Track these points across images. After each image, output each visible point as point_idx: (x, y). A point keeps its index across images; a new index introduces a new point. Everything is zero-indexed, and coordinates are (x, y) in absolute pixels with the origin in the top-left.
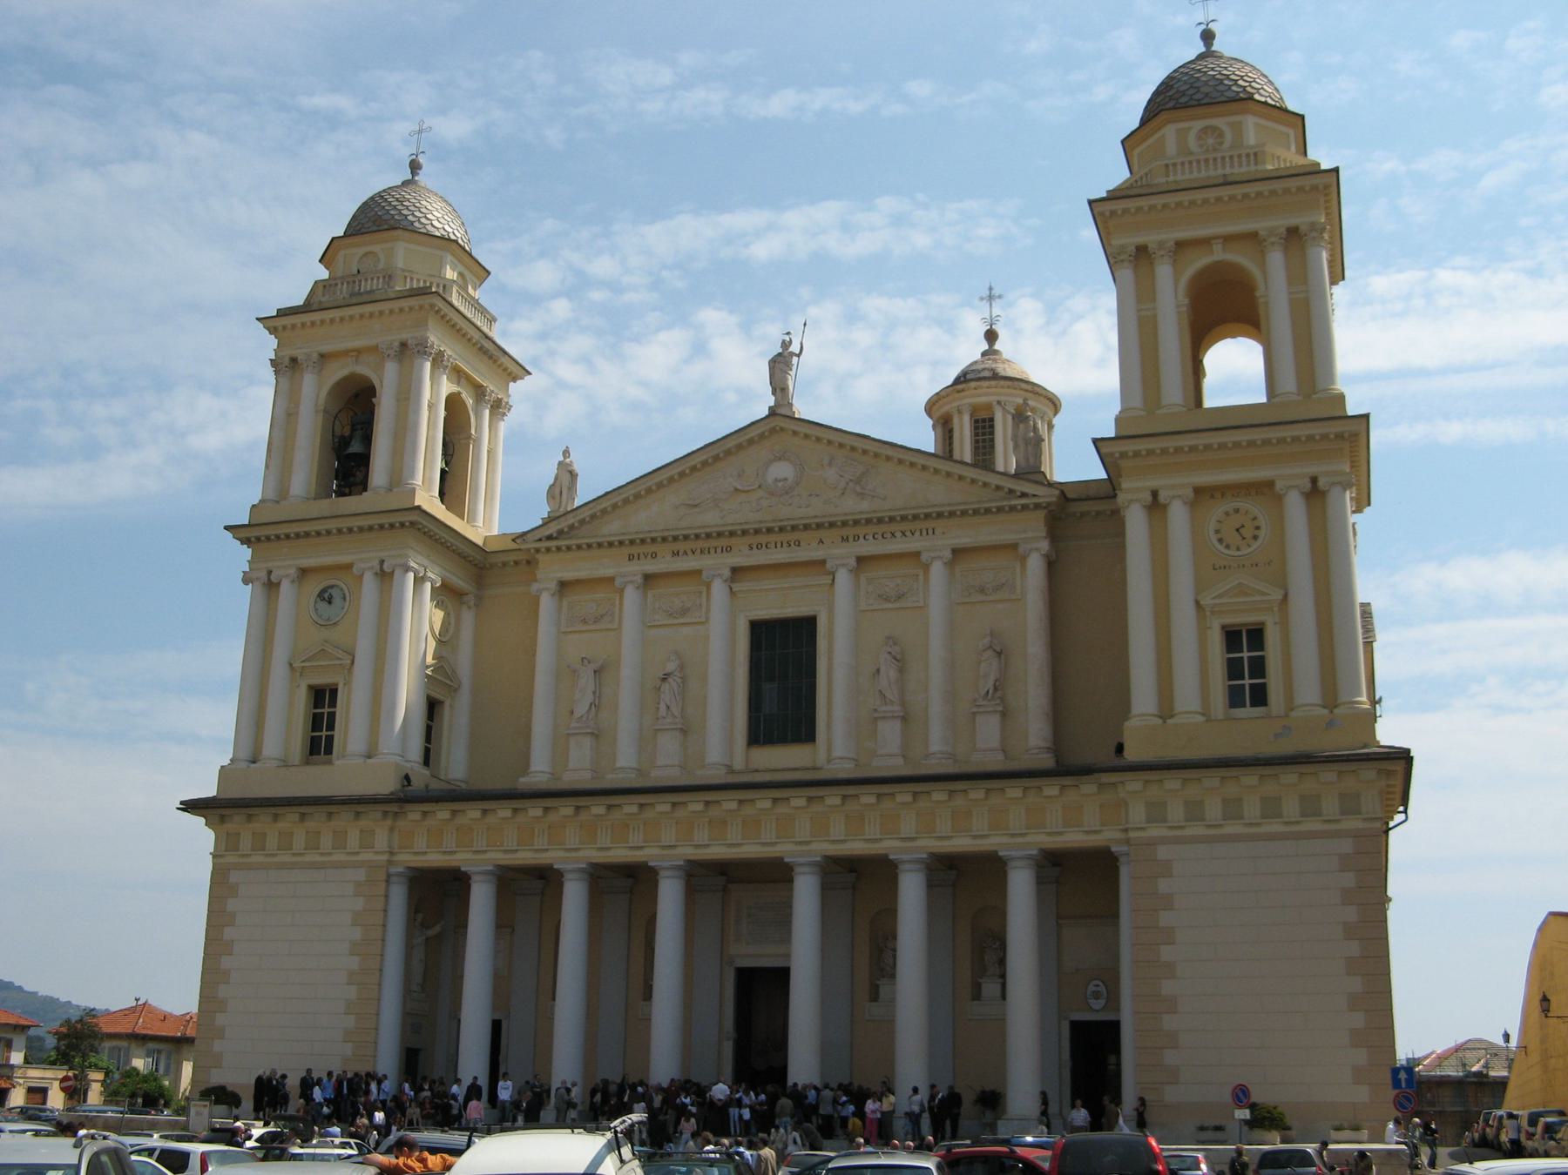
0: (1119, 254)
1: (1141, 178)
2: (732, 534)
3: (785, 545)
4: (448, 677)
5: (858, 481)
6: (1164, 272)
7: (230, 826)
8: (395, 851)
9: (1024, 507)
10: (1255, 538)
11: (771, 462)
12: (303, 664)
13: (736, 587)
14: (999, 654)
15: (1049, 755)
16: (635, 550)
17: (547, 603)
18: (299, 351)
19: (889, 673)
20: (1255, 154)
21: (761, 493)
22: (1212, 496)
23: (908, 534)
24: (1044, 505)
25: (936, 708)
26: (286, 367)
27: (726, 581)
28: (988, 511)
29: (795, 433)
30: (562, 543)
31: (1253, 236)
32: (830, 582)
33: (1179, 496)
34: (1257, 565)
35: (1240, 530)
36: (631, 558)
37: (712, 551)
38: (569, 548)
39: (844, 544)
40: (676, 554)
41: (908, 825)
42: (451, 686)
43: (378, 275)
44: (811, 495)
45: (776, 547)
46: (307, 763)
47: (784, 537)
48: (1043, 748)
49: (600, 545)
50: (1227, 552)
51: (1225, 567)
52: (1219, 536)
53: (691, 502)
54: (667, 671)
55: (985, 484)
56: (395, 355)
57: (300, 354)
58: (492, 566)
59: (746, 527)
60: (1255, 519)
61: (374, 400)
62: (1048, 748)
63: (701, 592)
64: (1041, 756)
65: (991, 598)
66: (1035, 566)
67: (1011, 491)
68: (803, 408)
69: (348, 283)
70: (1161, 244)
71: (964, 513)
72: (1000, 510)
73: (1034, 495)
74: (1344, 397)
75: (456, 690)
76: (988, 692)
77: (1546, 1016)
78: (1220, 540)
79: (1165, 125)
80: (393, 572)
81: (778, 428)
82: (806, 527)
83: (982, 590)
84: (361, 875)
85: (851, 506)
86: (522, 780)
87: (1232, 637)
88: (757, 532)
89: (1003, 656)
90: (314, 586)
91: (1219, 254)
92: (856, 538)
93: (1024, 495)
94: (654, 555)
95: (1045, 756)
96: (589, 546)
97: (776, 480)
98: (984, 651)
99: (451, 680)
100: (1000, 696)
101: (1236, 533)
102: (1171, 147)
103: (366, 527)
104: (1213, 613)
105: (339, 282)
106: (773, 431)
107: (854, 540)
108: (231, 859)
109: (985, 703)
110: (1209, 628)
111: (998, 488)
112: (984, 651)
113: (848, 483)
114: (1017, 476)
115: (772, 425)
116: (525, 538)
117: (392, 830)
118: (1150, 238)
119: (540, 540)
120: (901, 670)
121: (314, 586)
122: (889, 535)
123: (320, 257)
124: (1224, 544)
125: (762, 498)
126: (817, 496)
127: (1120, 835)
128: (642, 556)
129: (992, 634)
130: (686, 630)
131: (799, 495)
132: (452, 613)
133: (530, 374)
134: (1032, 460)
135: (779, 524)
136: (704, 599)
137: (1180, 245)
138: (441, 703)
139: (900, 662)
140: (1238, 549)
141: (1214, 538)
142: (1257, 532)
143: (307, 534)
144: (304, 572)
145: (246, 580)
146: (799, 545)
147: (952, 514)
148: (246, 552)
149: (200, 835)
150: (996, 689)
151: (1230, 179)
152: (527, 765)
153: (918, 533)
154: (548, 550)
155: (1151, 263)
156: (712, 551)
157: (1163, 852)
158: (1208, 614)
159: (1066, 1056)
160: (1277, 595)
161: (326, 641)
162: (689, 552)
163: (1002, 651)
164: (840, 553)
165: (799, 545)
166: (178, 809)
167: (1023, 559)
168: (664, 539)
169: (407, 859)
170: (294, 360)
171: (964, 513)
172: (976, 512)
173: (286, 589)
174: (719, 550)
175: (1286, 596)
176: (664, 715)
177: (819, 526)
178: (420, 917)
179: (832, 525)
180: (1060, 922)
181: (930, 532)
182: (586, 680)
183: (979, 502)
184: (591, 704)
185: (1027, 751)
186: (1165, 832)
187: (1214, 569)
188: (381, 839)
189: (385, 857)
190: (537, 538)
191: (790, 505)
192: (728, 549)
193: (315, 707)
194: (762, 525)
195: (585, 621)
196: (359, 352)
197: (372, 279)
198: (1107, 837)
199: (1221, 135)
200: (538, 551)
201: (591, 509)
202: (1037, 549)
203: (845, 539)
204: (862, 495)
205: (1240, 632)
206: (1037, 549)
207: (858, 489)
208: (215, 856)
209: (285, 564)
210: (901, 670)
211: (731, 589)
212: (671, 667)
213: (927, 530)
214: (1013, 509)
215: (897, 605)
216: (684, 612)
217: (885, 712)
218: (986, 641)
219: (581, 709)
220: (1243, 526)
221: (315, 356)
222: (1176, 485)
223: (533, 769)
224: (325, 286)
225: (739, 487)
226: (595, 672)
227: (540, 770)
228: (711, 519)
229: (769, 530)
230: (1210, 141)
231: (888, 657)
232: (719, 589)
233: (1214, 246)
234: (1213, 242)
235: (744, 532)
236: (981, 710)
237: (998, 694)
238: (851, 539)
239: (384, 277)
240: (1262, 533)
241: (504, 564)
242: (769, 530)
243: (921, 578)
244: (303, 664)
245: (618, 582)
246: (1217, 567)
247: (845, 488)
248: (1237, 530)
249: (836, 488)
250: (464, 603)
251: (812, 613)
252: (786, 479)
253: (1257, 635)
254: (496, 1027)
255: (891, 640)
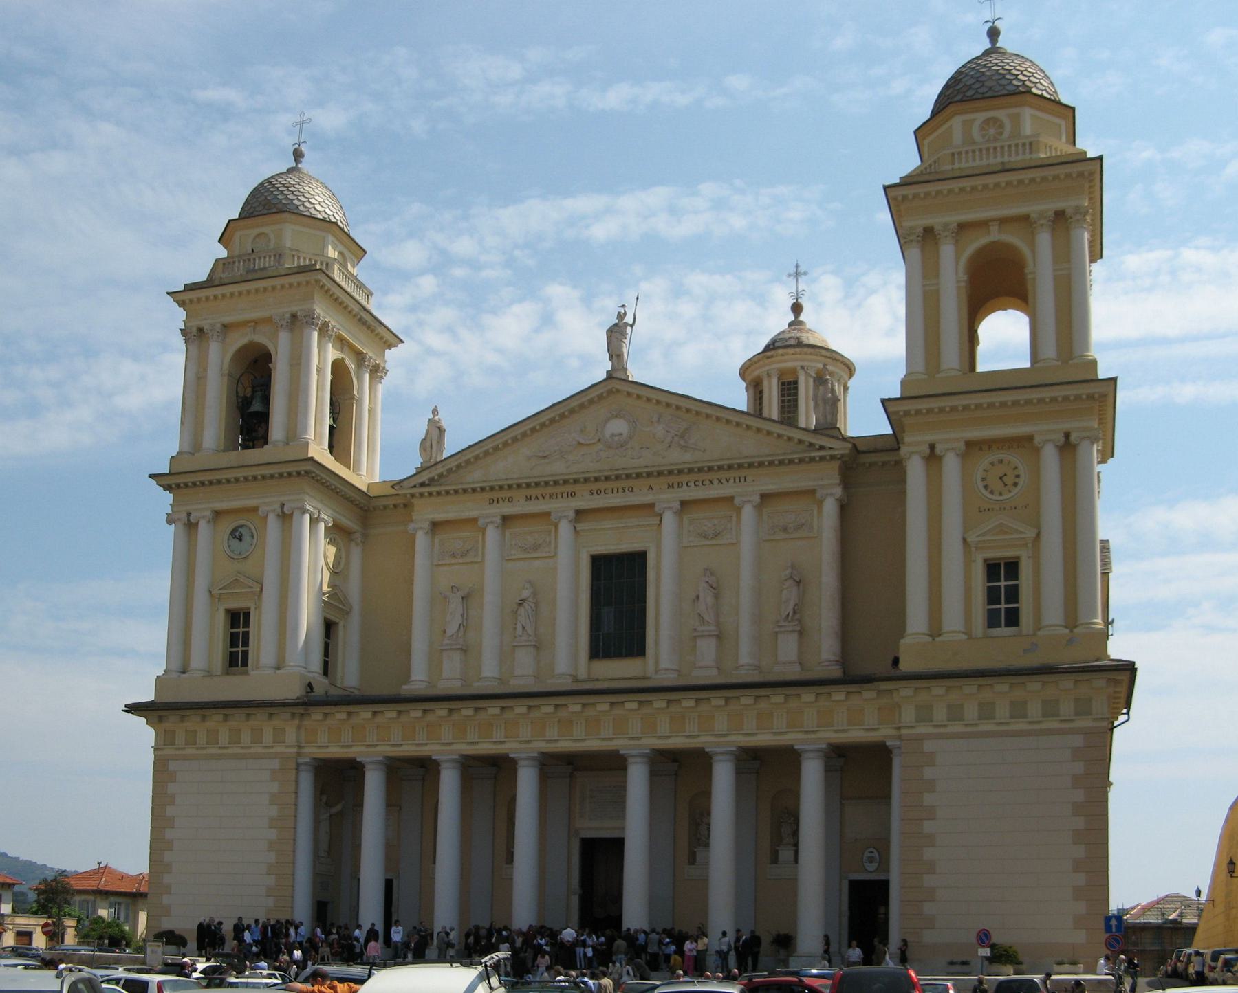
0: (909, 235)
1: (930, 165)
2: (576, 481)
3: (620, 490)
4: (341, 602)
5: (682, 436)
6: (947, 251)
7: (167, 725)
8: (302, 745)
9: (822, 458)
10: (1015, 484)
11: (607, 420)
12: (221, 592)
13: (580, 527)
14: (798, 583)
15: (838, 667)
16: (495, 495)
17: (421, 540)
18: (204, 322)
19: (707, 598)
20: (1031, 144)
21: (600, 446)
22: (981, 449)
23: (724, 481)
24: (839, 456)
25: (745, 628)
26: (195, 336)
27: (571, 521)
28: (791, 462)
29: (629, 394)
30: (433, 489)
31: (1025, 219)
32: (658, 522)
33: (952, 449)
34: (1015, 508)
35: (1003, 478)
36: (491, 502)
37: (559, 496)
38: (439, 493)
39: (671, 490)
40: (529, 498)
41: (721, 724)
42: (343, 610)
43: (269, 254)
44: (642, 448)
45: (613, 493)
46: (228, 674)
47: (620, 484)
48: (833, 661)
49: (465, 491)
50: (990, 496)
51: (989, 510)
52: (985, 483)
53: (540, 454)
54: (523, 597)
55: (789, 439)
56: (287, 326)
57: (205, 324)
58: (375, 508)
59: (587, 475)
60: (1016, 468)
61: (270, 365)
62: (837, 661)
63: (550, 531)
64: (830, 668)
65: (792, 536)
66: (830, 508)
67: (811, 445)
68: (636, 373)
69: (244, 261)
70: (946, 226)
71: (771, 463)
72: (801, 461)
73: (830, 448)
74: (1096, 362)
75: (348, 613)
76: (788, 614)
77: (1232, 876)
78: (986, 487)
79: (953, 116)
80: (292, 513)
81: (614, 390)
82: (638, 476)
83: (785, 529)
84: (275, 764)
85: (677, 457)
86: (404, 687)
87: (992, 569)
88: (597, 479)
89: (801, 585)
90: (227, 526)
91: (995, 235)
92: (680, 485)
93: (822, 448)
94: (511, 500)
95: (833, 667)
96: (456, 492)
97: (613, 435)
98: (786, 580)
99: (344, 605)
100: (798, 619)
101: (999, 480)
102: (957, 137)
103: (268, 475)
104: (977, 549)
105: (236, 260)
106: (610, 392)
107: (678, 487)
108: (169, 751)
109: (786, 624)
110: (974, 561)
111: (800, 442)
112: (786, 580)
113: (673, 438)
114: (817, 431)
115: (609, 387)
116: (402, 484)
117: (299, 727)
118: (935, 221)
119: (415, 486)
120: (717, 597)
121: (227, 526)
122: (708, 482)
123: (218, 238)
124: (989, 490)
125: (601, 450)
126: (648, 448)
127: (893, 732)
128: (500, 500)
129: (793, 567)
130: (537, 563)
131: (632, 448)
132: (343, 549)
133: (403, 342)
134: (829, 417)
135: (616, 473)
136: (553, 537)
137: (962, 226)
138: (336, 624)
139: (716, 590)
140: (1001, 494)
141: (980, 485)
142: (1017, 480)
143: (219, 482)
144: (217, 514)
145: (170, 521)
146: (632, 491)
147: (761, 464)
148: (168, 497)
149: (143, 732)
150: (795, 612)
151: (1008, 167)
152: (409, 676)
153: (732, 481)
154: (422, 495)
155: (937, 243)
156: (559, 496)
157: (928, 746)
158: (973, 549)
159: (845, 907)
160: (1031, 533)
161: (238, 572)
162: (540, 497)
163: (800, 581)
164: (667, 498)
165: (632, 491)
166: (123, 711)
167: (820, 503)
168: (519, 486)
169: (312, 751)
170: (201, 330)
171: (771, 463)
172: (781, 463)
173: (204, 529)
174: (565, 495)
175: (1038, 535)
176: (520, 634)
177: (649, 475)
178: (324, 798)
179: (660, 473)
180: (843, 802)
181: (742, 480)
182: (456, 605)
183: (785, 454)
184: (460, 625)
185: (819, 663)
186: (931, 730)
187: (980, 511)
188: (291, 735)
189: (295, 750)
190: (412, 485)
191: (625, 456)
192: (573, 494)
193: (232, 628)
194: (601, 474)
195: (453, 556)
196: (256, 322)
197: (265, 257)
198: (882, 733)
199: (1001, 126)
200: (413, 496)
201: (456, 460)
202: (832, 495)
203: (671, 486)
204: (685, 448)
205: (999, 565)
206: (832, 495)
207: (682, 443)
208: (156, 749)
209: (202, 508)
210: (717, 597)
211: (575, 528)
212: (525, 594)
213: (740, 478)
214: (812, 460)
215: (714, 542)
216: (536, 547)
217: (702, 631)
218: (788, 572)
219: (452, 629)
220: (1005, 475)
221: (219, 326)
222: (950, 439)
223: (413, 678)
224: (224, 264)
225: (582, 441)
226: (463, 598)
227: (419, 679)
228: (558, 468)
229: (607, 478)
230: (992, 131)
231: (706, 585)
232: (565, 528)
233: (991, 228)
234: (991, 223)
235: (586, 480)
236: (783, 629)
237: (797, 616)
238: (676, 485)
239: (275, 256)
240: (1021, 481)
241: (385, 507)
242: (607, 478)
243: (734, 519)
244: (221, 592)
245: (481, 522)
246: (982, 509)
247: (671, 442)
248: (1001, 478)
249: (663, 442)
250: (352, 540)
251: (643, 549)
252: (621, 434)
253: (1012, 568)
254: (389, 885)
255: (708, 571)
